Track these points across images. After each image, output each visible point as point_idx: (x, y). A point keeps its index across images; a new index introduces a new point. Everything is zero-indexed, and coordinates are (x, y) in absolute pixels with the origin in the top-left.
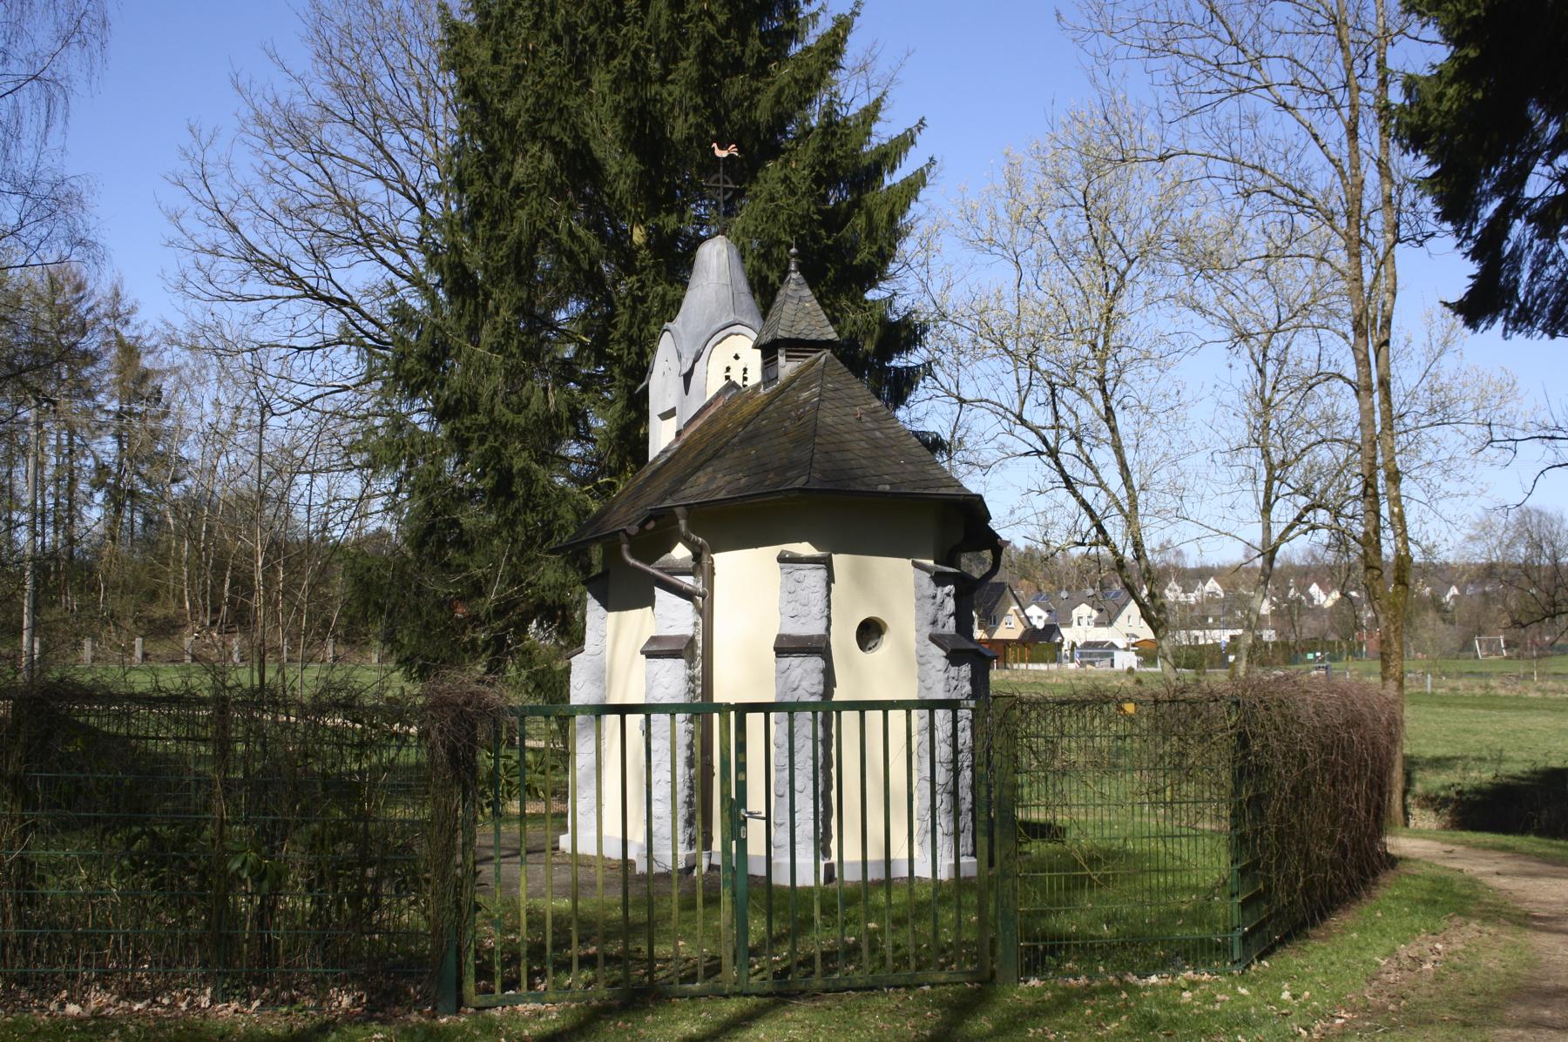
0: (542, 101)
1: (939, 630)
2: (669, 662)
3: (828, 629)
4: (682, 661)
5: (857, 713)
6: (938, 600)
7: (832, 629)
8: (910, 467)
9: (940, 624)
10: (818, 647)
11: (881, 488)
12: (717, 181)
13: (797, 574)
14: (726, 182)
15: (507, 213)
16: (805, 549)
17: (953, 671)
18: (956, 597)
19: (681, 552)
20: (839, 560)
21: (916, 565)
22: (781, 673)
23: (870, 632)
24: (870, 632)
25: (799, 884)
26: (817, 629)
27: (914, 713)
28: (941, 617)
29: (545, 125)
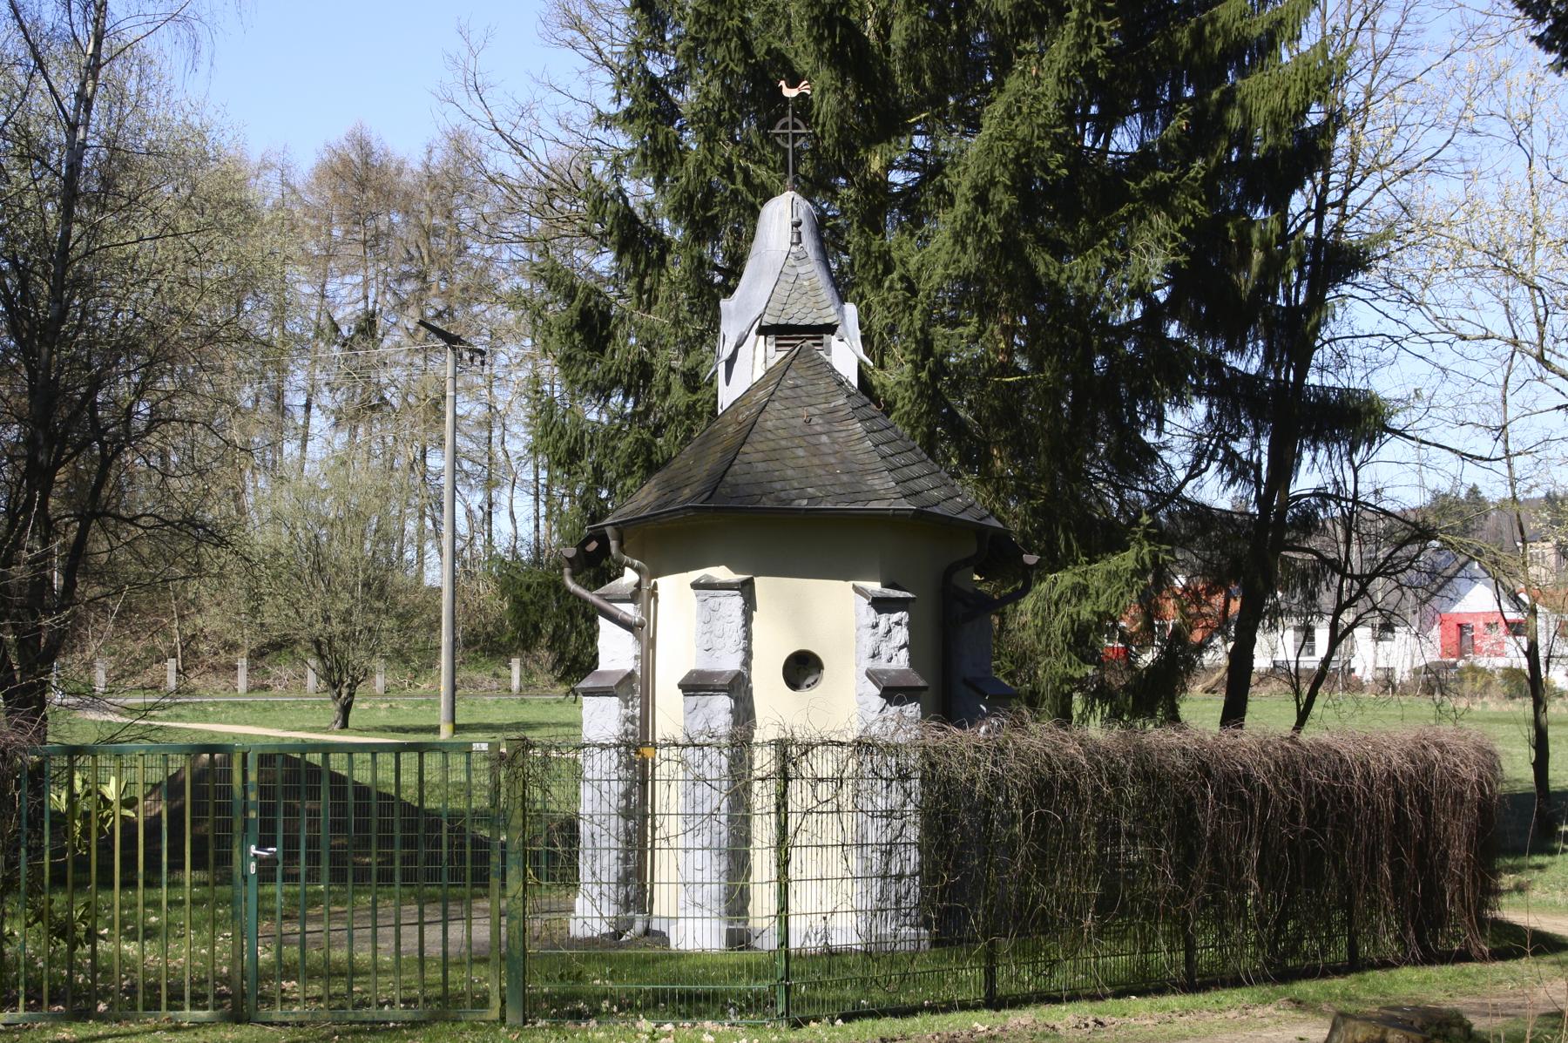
0: (703, 19)
1: (881, 664)
2: (604, 700)
3: (747, 663)
4: (616, 699)
5: (415, 755)
6: (882, 628)
7: (754, 663)
8: (845, 478)
9: (884, 657)
10: (738, 687)
11: (796, 504)
12: (785, 126)
13: (711, 602)
14: (796, 126)
15: (676, 155)
16: (721, 573)
17: (893, 710)
18: (910, 626)
19: (630, 577)
20: (761, 583)
21: (857, 589)
22: (691, 712)
23: (802, 669)
24: (802, 669)
25: (795, 943)
26: (730, 663)
27: (404, 756)
28: (886, 650)
29: (710, 47)
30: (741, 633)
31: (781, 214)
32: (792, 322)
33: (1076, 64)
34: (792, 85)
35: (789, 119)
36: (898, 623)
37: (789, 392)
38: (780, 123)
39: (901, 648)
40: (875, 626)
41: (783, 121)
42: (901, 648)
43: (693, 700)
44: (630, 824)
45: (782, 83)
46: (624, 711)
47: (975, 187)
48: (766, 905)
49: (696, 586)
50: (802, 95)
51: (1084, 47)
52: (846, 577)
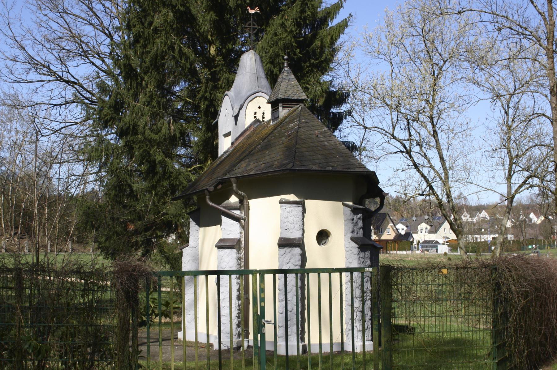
1: (355, 235)
2: (228, 251)
3: (303, 235)
4: (235, 251)
8: (341, 159)
10: (299, 244)
11: (327, 169)
12: (250, 25)
15: (151, 41)
16: (292, 197)
19: (234, 199)
30: (301, 222)
31: (251, 59)
32: (290, 98)
33: (300, 18)
34: (252, 9)
35: (251, 22)
36: (359, 219)
37: (304, 125)
38: (248, 23)
39: (360, 228)
40: (353, 220)
41: (249, 22)
42: (360, 228)
43: (283, 250)
44: (240, 302)
45: (248, 8)
46: (237, 255)
47: (271, 58)
48: (202, 329)
49: (281, 202)
50: (256, 13)
51: (303, 11)
52: (340, 200)
